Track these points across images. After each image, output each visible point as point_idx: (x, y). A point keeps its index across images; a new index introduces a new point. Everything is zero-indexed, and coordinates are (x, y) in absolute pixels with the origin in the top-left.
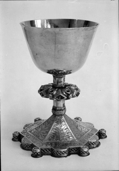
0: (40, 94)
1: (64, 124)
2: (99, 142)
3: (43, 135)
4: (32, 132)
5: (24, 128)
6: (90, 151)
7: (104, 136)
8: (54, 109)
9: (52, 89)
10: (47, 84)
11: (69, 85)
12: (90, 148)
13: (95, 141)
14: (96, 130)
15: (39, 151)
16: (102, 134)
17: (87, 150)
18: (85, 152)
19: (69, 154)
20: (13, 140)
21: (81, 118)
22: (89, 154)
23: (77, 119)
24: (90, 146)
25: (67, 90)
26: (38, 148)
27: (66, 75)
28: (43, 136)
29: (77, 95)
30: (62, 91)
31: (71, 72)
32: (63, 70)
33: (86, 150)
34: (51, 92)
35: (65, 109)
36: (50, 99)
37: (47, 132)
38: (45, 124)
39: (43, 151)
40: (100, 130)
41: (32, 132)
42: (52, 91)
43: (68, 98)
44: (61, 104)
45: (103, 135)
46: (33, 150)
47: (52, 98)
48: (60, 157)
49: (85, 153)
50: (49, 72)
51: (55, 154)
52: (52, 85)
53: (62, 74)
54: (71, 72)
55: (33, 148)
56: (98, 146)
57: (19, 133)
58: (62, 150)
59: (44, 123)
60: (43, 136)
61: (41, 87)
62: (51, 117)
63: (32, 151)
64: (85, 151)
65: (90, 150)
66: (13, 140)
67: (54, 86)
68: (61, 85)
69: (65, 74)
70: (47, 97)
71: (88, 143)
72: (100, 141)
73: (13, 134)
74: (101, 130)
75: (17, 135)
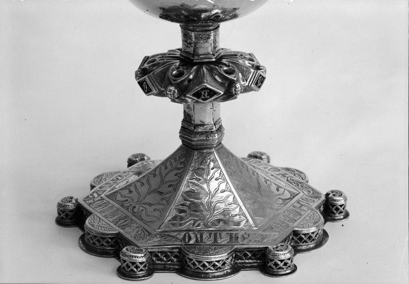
0: (141, 84)
1: (217, 175)
2: (325, 234)
3: (131, 192)
4: (119, 197)
5: (92, 187)
6: (299, 259)
7: (341, 212)
8: (189, 127)
9: (178, 68)
10: (165, 50)
11: (234, 55)
12: (296, 250)
13: (313, 229)
14: (316, 194)
15: (141, 258)
16: (333, 206)
17: (288, 256)
18: (282, 261)
19: (235, 270)
20: (61, 222)
21: (268, 153)
22: (294, 269)
23: (255, 156)
24: (297, 241)
25: (225, 68)
26: (140, 251)
27: (222, 25)
28: (279, 192)
29: (260, 82)
30: (211, 71)
31: (237, 12)
32: (211, 10)
33: (284, 255)
34: (176, 76)
35: (220, 129)
36: (173, 100)
37: (176, 188)
38: (157, 173)
39: (156, 256)
40: (327, 195)
41: (119, 197)
42: (180, 74)
43: (229, 95)
44: (207, 114)
45: (337, 209)
46: (125, 255)
47: (179, 98)
48: (206, 277)
49: (281, 265)
50: (168, 14)
51: (189, 266)
52: (178, 54)
53: (209, 19)
54: (237, 12)
55: (124, 249)
56: (319, 245)
57: (76, 200)
58: (214, 258)
59: (157, 168)
60: (279, 192)
61: (143, 64)
62: (176, 152)
63: (118, 258)
64: (282, 257)
65: (298, 255)
66: (61, 222)
67: (187, 59)
68: (209, 54)
69: (217, 19)
70: (161, 94)
71: (296, 233)
72: (329, 227)
73: (59, 205)
74: (331, 195)
75: (71, 206)
